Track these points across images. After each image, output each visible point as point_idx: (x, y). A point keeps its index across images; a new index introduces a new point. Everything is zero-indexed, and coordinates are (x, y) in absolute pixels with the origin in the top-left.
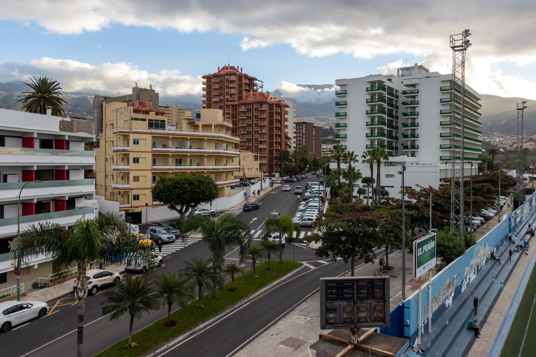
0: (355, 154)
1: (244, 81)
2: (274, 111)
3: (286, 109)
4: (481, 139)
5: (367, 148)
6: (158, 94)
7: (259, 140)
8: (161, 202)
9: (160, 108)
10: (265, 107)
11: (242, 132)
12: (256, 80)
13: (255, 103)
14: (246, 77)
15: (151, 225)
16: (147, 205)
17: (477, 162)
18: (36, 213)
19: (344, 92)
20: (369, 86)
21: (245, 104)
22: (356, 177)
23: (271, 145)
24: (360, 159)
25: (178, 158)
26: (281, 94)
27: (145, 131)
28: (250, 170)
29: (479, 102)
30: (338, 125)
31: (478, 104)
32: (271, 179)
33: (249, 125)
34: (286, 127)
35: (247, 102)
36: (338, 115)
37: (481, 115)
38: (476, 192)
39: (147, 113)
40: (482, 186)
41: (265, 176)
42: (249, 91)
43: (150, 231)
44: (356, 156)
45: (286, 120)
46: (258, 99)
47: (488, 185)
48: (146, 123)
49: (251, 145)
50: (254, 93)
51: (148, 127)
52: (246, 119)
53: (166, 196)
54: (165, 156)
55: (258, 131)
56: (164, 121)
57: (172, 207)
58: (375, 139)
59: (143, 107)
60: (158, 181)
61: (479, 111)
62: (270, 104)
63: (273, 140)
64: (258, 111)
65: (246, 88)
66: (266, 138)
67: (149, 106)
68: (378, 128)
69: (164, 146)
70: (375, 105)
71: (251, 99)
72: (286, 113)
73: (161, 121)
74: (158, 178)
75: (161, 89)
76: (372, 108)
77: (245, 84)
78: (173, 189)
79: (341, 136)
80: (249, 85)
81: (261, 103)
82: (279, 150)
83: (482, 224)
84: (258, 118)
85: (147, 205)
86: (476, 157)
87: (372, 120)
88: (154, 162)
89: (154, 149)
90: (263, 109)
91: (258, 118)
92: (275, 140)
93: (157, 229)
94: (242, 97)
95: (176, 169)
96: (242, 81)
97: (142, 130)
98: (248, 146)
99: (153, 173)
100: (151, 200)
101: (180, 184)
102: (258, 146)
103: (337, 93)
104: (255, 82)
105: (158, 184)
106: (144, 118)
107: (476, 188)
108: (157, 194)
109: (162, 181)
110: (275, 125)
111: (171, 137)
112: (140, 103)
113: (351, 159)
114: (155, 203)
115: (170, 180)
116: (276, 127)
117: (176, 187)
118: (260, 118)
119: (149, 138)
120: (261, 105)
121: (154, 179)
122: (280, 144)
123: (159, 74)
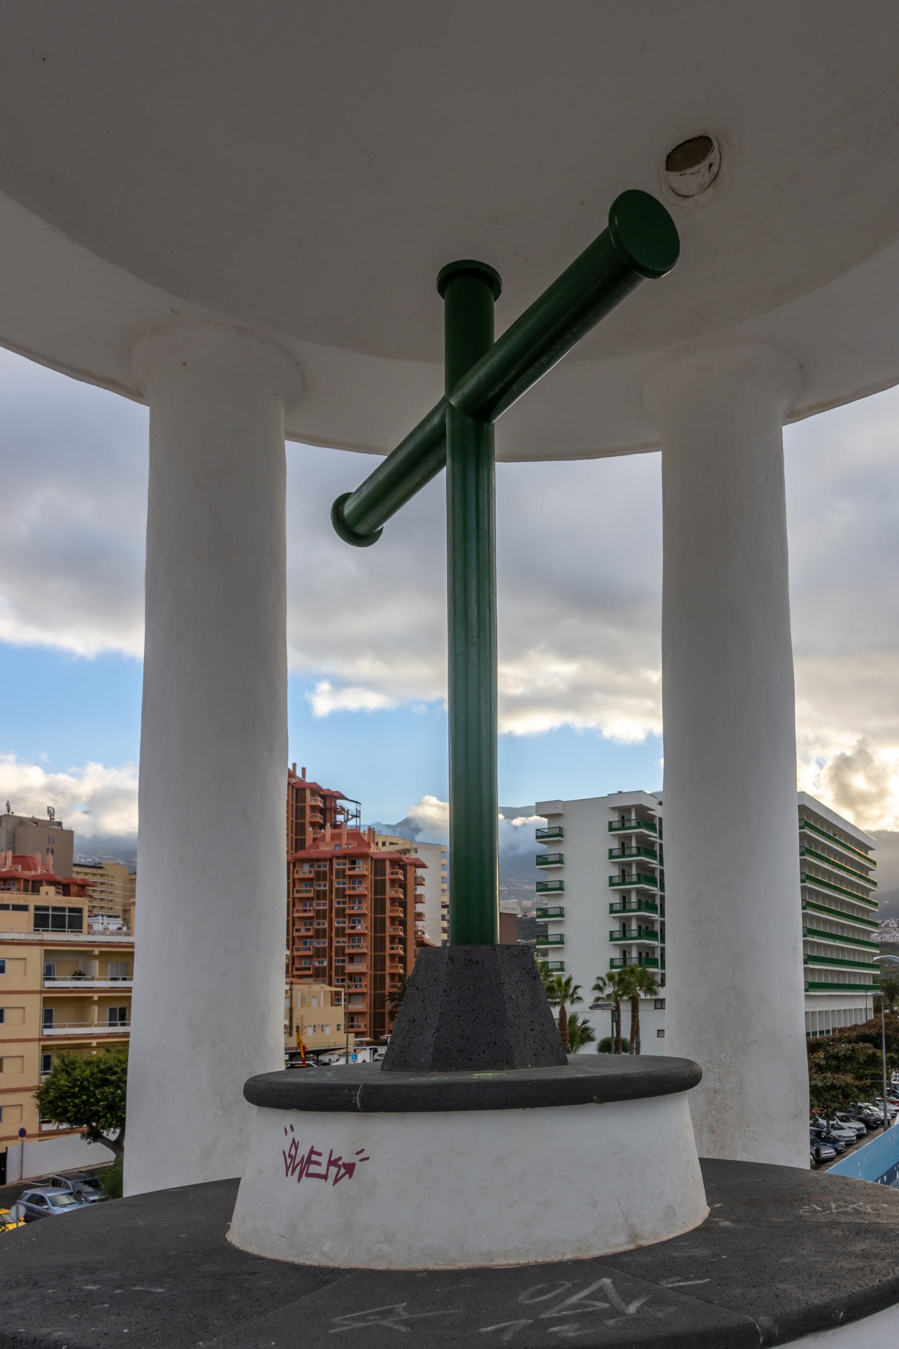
0: (573, 984)
1: (310, 801)
2: (388, 876)
3: (420, 872)
4: (875, 937)
5: (612, 967)
6: (71, 833)
7: (347, 951)
8: (61, 1122)
9: (75, 869)
10: (363, 868)
11: (303, 933)
12: (343, 797)
13: (338, 857)
14: (316, 790)
15: (30, 1187)
16: (22, 1133)
17: (869, 993)
18: (35, 915)
19: (557, 831)
20: (615, 817)
21: (311, 861)
22: (578, 1039)
23: (379, 963)
24: (588, 996)
25: (118, 1006)
26: (417, 830)
27: (23, 937)
28: (318, 1030)
29: (871, 855)
30: (544, 913)
31: (869, 860)
32: (375, 1051)
33: (320, 915)
34: (419, 916)
35: (315, 856)
36: (542, 887)
37: (875, 884)
38: (837, 1063)
39: (34, 886)
40: (853, 1051)
41: (361, 1044)
42: (322, 826)
43: (29, 1200)
44: (577, 987)
45: (419, 899)
46: (344, 846)
47: (865, 1048)
48: (28, 918)
49: (326, 964)
50: (336, 831)
51: (32, 928)
52: (311, 899)
53: (75, 1105)
54: (79, 1004)
55: (344, 929)
56: (80, 910)
57: (95, 1136)
58: (630, 945)
59: (26, 867)
60: (56, 1069)
61: (871, 876)
62: (376, 861)
63: (384, 949)
64: (344, 876)
65: (314, 819)
66: (365, 946)
67: (44, 864)
68: (639, 918)
69: (79, 975)
70: (629, 864)
71: (326, 848)
72: (419, 882)
73: (71, 910)
74: (55, 1061)
75: (86, 817)
76: (623, 871)
77: (314, 808)
78: (96, 1087)
79: (551, 939)
80: (323, 811)
81: (353, 859)
82: (400, 976)
83: (860, 1137)
84: (344, 896)
85: (22, 1133)
86: (869, 982)
87: (625, 900)
88: (48, 1018)
89: (48, 984)
90: (357, 872)
91: (344, 896)
92: (388, 951)
93: (49, 1194)
94: (303, 842)
95: (109, 1035)
96: (304, 802)
97: (16, 936)
98: (317, 969)
99: (44, 1048)
100: (37, 1119)
101: (115, 1073)
102: (343, 968)
103: (541, 836)
104: (340, 802)
105: (54, 1076)
106: (22, 903)
107: (840, 1054)
108: (50, 1102)
109: (68, 1068)
110: (388, 914)
111: (97, 951)
112: (17, 859)
113: (566, 996)
114: (46, 1127)
115: (89, 1063)
116: (393, 919)
117: (105, 1082)
118: (350, 896)
119: (35, 956)
120: (354, 863)
121: (46, 1063)
122: (403, 960)
123: (80, 776)
